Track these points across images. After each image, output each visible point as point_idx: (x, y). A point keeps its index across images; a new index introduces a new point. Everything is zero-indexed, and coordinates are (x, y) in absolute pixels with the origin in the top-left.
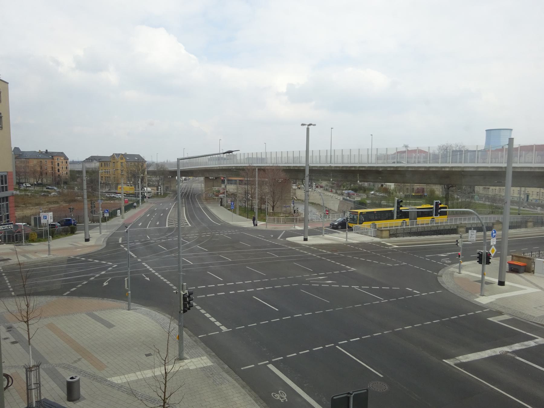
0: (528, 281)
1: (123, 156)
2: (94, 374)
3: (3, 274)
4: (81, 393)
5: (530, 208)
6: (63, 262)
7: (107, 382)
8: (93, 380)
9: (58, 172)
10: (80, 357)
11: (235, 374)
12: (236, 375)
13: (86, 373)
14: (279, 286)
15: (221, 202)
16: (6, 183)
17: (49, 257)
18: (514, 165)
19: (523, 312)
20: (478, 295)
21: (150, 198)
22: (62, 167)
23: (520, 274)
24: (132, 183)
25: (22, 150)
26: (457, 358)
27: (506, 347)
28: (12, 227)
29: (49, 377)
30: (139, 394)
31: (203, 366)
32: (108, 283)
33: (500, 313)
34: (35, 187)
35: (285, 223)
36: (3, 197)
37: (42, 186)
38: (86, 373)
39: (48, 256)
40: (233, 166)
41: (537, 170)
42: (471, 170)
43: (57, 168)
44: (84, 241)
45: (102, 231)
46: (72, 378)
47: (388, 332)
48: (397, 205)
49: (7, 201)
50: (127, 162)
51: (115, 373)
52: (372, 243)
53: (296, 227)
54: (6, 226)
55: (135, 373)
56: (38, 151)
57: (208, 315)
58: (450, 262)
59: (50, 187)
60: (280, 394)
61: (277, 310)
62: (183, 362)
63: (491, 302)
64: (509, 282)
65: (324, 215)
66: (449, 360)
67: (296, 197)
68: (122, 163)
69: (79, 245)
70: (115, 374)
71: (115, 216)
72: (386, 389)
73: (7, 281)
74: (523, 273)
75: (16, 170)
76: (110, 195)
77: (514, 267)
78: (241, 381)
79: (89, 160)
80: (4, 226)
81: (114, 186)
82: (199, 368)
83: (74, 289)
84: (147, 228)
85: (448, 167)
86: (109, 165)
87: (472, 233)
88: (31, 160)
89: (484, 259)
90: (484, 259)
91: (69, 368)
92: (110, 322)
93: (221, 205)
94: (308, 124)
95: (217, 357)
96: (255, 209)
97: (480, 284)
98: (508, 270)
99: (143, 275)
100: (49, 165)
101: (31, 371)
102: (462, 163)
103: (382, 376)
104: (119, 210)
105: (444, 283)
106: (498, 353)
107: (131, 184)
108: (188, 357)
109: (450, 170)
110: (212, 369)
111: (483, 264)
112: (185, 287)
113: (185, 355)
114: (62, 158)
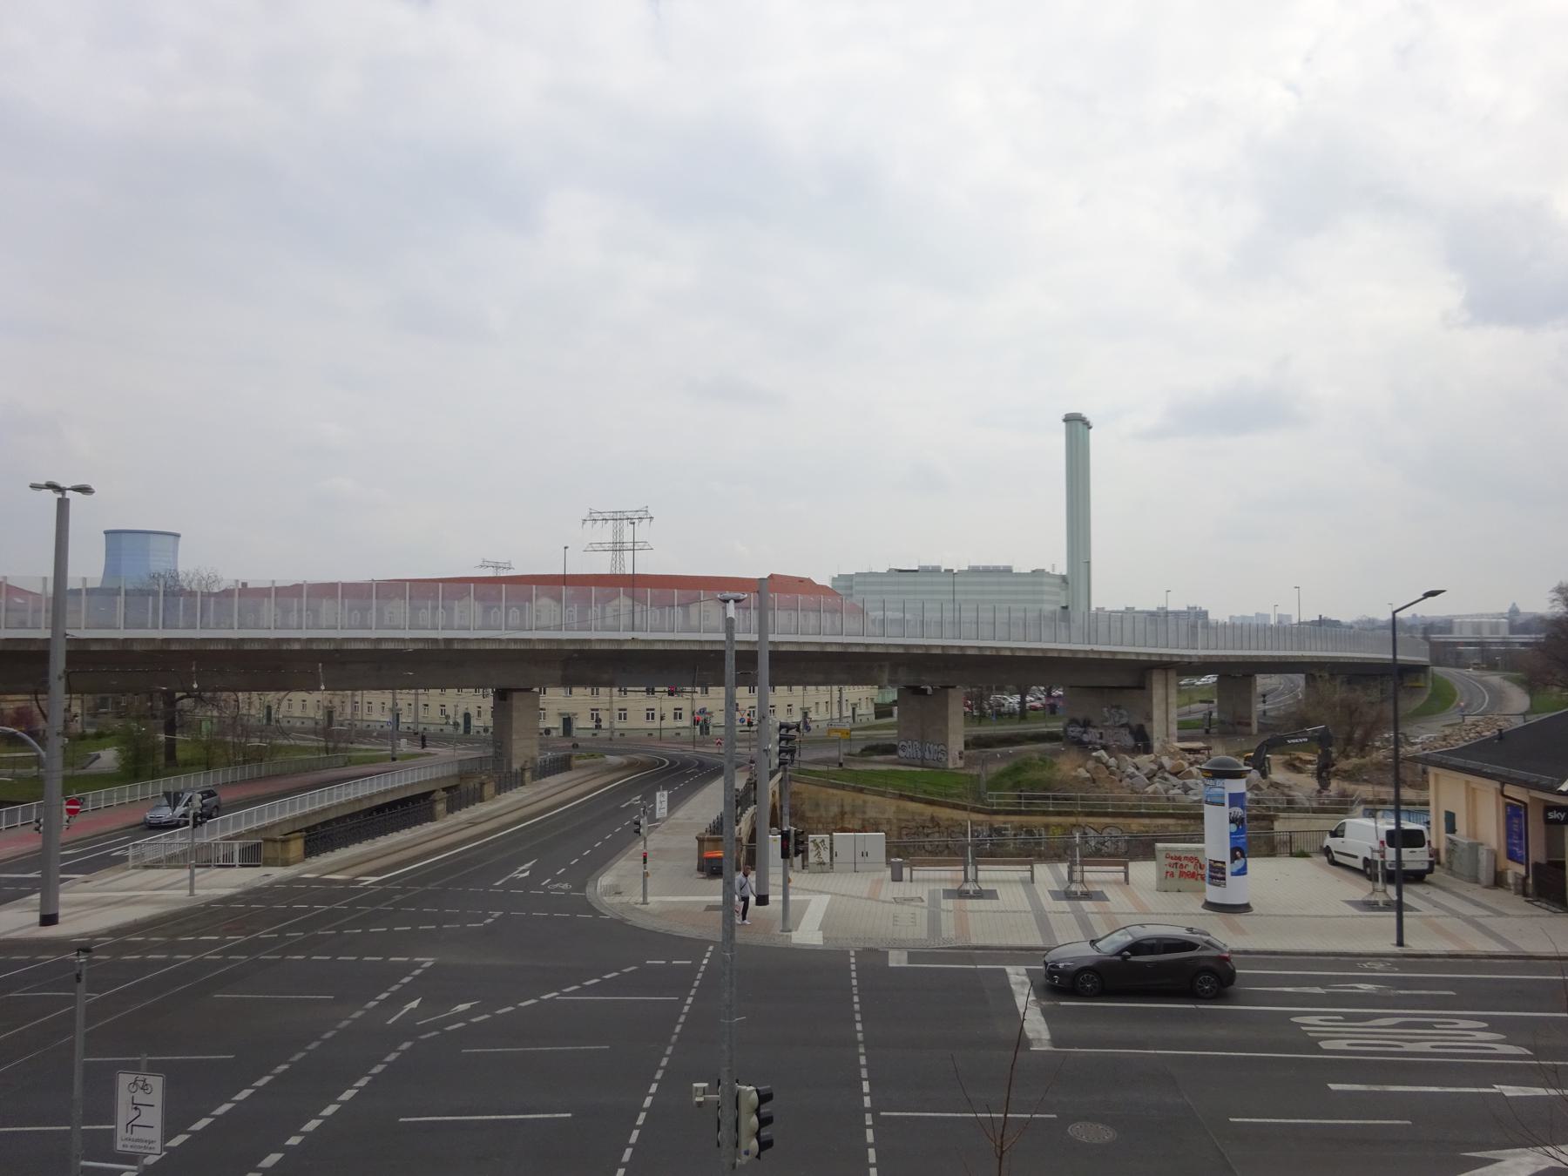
18: (772, 638)
41: (512, 646)
42: (362, 646)
85: (298, 640)
102: (195, 628)
109: (304, 648)
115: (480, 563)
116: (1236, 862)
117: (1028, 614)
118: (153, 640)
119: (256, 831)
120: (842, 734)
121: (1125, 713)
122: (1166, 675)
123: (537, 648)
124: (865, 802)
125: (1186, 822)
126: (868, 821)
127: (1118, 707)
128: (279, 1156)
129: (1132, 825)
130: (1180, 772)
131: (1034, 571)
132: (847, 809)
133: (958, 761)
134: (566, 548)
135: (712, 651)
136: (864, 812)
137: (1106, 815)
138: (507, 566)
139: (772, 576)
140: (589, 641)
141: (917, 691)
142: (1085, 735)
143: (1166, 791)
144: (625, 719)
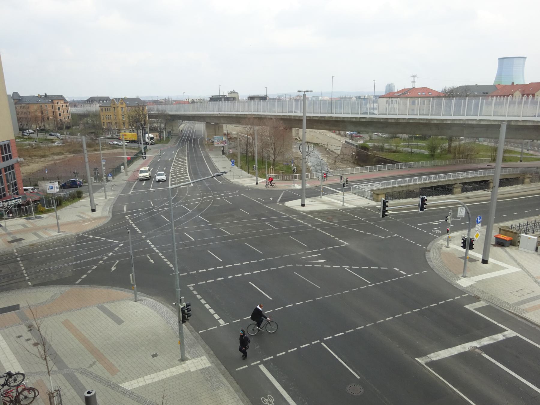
0: (511, 257)
1: (123, 101)
2: (108, 379)
3: (19, 259)
4: (97, 401)
5: (534, 150)
6: (73, 242)
7: (119, 389)
8: (107, 386)
9: (59, 116)
10: (95, 360)
11: (230, 375)
12: (231, 377)
13: (101, 379)
14: (274, 267)
15: (223, 151)
16: (10, 152)
17: (59, 235)
19: (499, 297)
20: (460, 276)
21: (152, 144)
22: (63, 111)
23: (505, 248)
24: (134, 128)
25: (21, 95)
26: (428, 356)
27: (475, 342)
28: (21, 201)
29: (69, 384)
30: (148, 401)
31: (202, 368)
32: (116, 268)
33: (477, 299)
34: (38, 133)
35: (285, 180)
36: (9, 166)
37: (45, 131)
38: (101, 379)
39: (58, 234)
40: (233, 114)
43: (58, 112)
44: (91, 211)
45: (108, 193)
46: (89, 393)
47: (370, 325)
48: (383, 214)
49: (13, 169)
50: (127, 107)
51: (126, 377)
52: (368, 207)
53: (295, 185)
54: (15, 200)
55: (143, 377)
56: (38, 95)
57: (207, 306)
58: (440, 232)
59: (53, 134)
60: (268, 399)
61: (271, 299)
62: (185, 363)
63: (471, 286)
64: (493, 258)
65: (322, 177)
66: (421, 358)
67: (299, 138)
68: (122, 108)
69: (87, 217)
70: (126, 379)
71: (118, 172)
72: (361, 392)
73: (23, 268)
74: (509, 246)
75: (17, 116)
76: (113, 142)
77: (500, 241)
78: (236, 384)
79: (87, 102)
80: (13, 201)
81: (116, 132)
82: (199, 370)
83: (85, 276)
84: (150, 189)
85: (450, 120)
86: (110, 111)
87: (462, 210)
88: (31, 105)
89: (468, 244)
90: (468, 244)
91: (86, 373)
92: (120, 316)
93: (224, 153)
94: (305, 90)
95: (215, 356)
96: (255, 168)
97: (463, 261)
98: (494, 243)
99: (148, 256)
100: (50, 110)
101: (53, 397)
103: (359, 378)
104: (123, 166)
105: (431, 260)
106: (467, 349)
107: (133, 129)
108: (189, 358)
109: (451, 123)
110: (210, 371)
111: (466, 248)
112: (183, 300)
113: (187, 356)
114: (62, 102)
117: (343, 195)
118: (405, 119)
119: (470, 178)
128: (82, 277)
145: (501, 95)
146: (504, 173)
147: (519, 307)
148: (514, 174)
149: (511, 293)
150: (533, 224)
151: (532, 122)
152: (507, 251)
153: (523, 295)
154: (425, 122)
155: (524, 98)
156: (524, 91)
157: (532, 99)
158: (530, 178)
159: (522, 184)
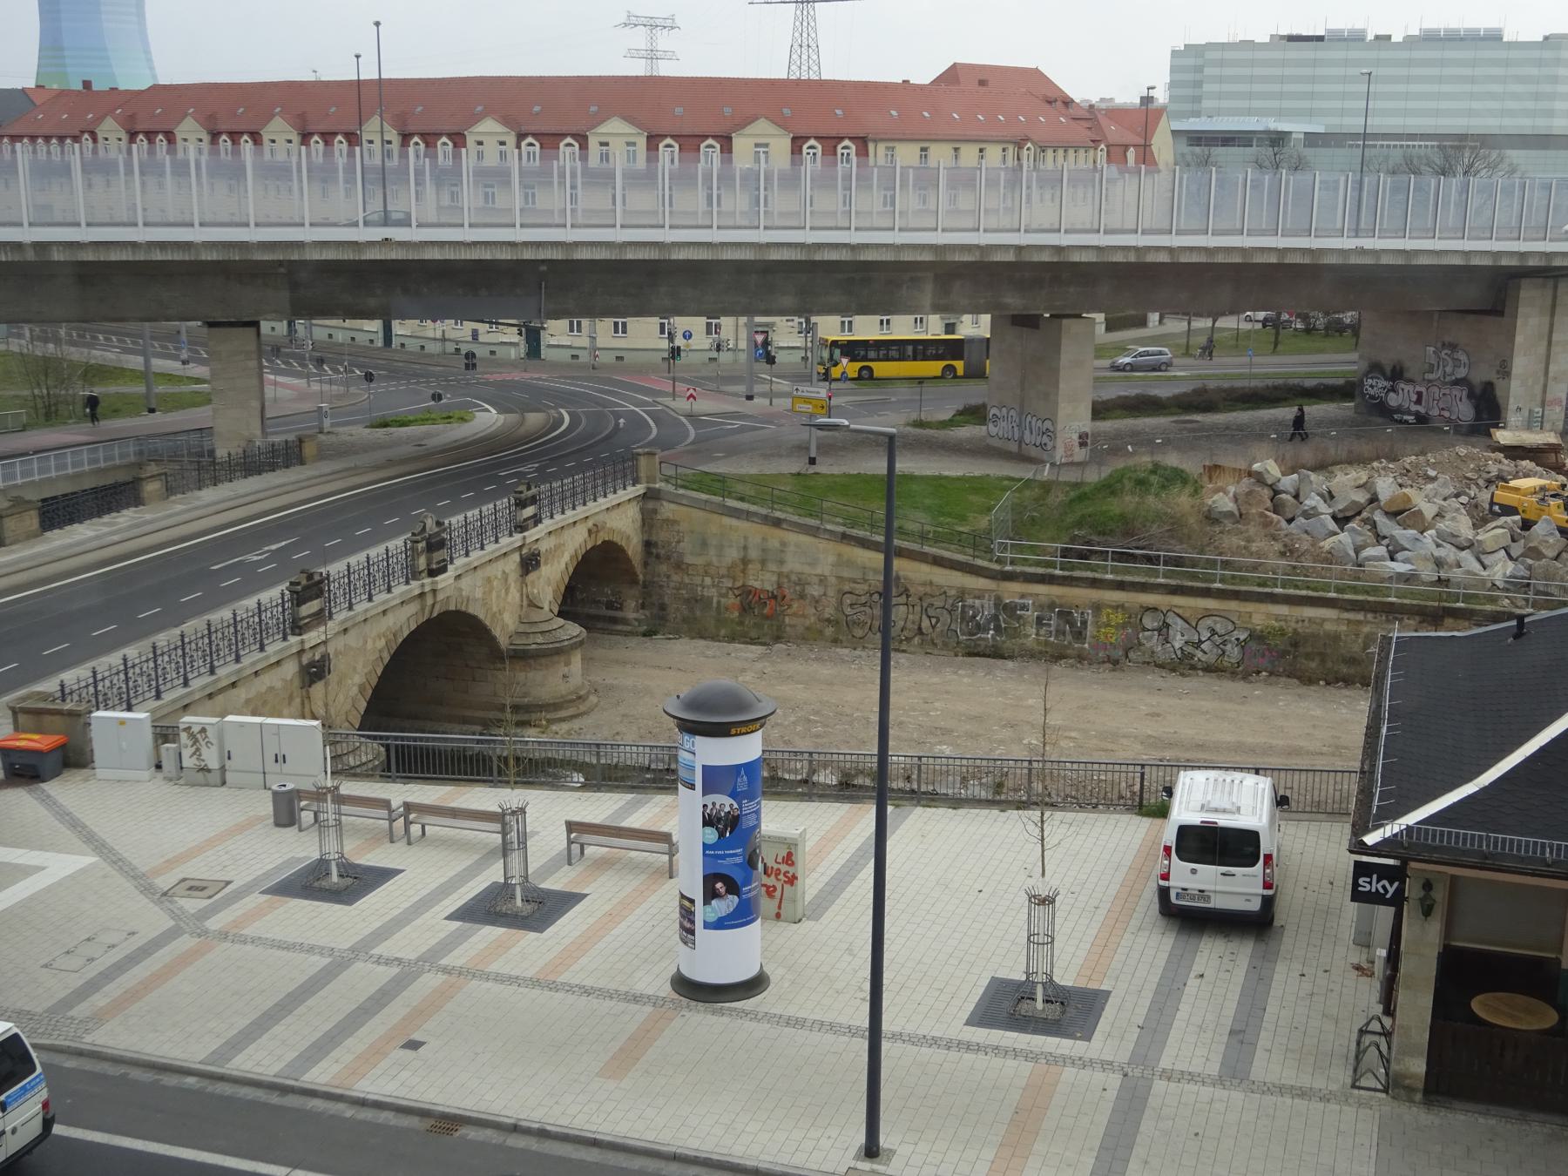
41: (158, 256)
115: (624, 19)
116: (714, 902)
120: (815, 406)
121: (1463, 358)
122: (1555, 288)
123: (203, 258)
124: (783, 544)
125: (1360, 616)
126: (787, 576)
127: (1453, 347)
129: (1254, 616)
130: (1401, 512)
131: (1546, 38)
132: (754, 554)
133: (1077, 449)
134: (358, 57)
135: (543, 261)
136: (782, 562)
137: (1206, 593)
138: (669, 23)
139: (953, 75)
140: (299, 245)
141: (1026, 321)
142: (1392, 394)
143: (1357, 551)
144: (624, 332)
145: (63, 132)
146: (89, 464)
147: (70, 1014)
148: (116, 468)
149: (46, 966)
150: (147, 661)
151: (560, 248)
152: (49, 796)
153: (91, 960)
154: (1275, 261)
155: (411, 150)
156: (132, 118)
157: (210, 153)
158: (163, 477)
159: (136, 506)
